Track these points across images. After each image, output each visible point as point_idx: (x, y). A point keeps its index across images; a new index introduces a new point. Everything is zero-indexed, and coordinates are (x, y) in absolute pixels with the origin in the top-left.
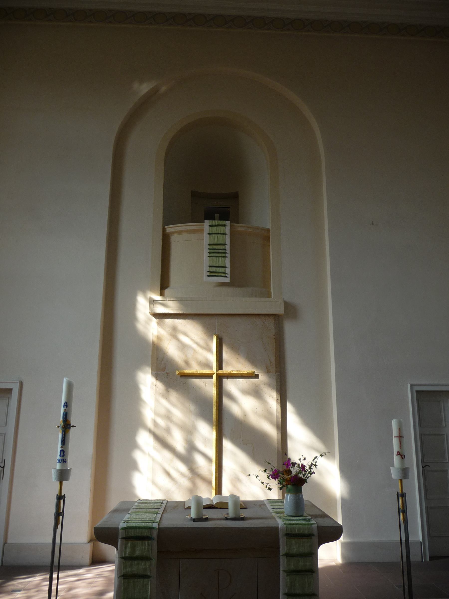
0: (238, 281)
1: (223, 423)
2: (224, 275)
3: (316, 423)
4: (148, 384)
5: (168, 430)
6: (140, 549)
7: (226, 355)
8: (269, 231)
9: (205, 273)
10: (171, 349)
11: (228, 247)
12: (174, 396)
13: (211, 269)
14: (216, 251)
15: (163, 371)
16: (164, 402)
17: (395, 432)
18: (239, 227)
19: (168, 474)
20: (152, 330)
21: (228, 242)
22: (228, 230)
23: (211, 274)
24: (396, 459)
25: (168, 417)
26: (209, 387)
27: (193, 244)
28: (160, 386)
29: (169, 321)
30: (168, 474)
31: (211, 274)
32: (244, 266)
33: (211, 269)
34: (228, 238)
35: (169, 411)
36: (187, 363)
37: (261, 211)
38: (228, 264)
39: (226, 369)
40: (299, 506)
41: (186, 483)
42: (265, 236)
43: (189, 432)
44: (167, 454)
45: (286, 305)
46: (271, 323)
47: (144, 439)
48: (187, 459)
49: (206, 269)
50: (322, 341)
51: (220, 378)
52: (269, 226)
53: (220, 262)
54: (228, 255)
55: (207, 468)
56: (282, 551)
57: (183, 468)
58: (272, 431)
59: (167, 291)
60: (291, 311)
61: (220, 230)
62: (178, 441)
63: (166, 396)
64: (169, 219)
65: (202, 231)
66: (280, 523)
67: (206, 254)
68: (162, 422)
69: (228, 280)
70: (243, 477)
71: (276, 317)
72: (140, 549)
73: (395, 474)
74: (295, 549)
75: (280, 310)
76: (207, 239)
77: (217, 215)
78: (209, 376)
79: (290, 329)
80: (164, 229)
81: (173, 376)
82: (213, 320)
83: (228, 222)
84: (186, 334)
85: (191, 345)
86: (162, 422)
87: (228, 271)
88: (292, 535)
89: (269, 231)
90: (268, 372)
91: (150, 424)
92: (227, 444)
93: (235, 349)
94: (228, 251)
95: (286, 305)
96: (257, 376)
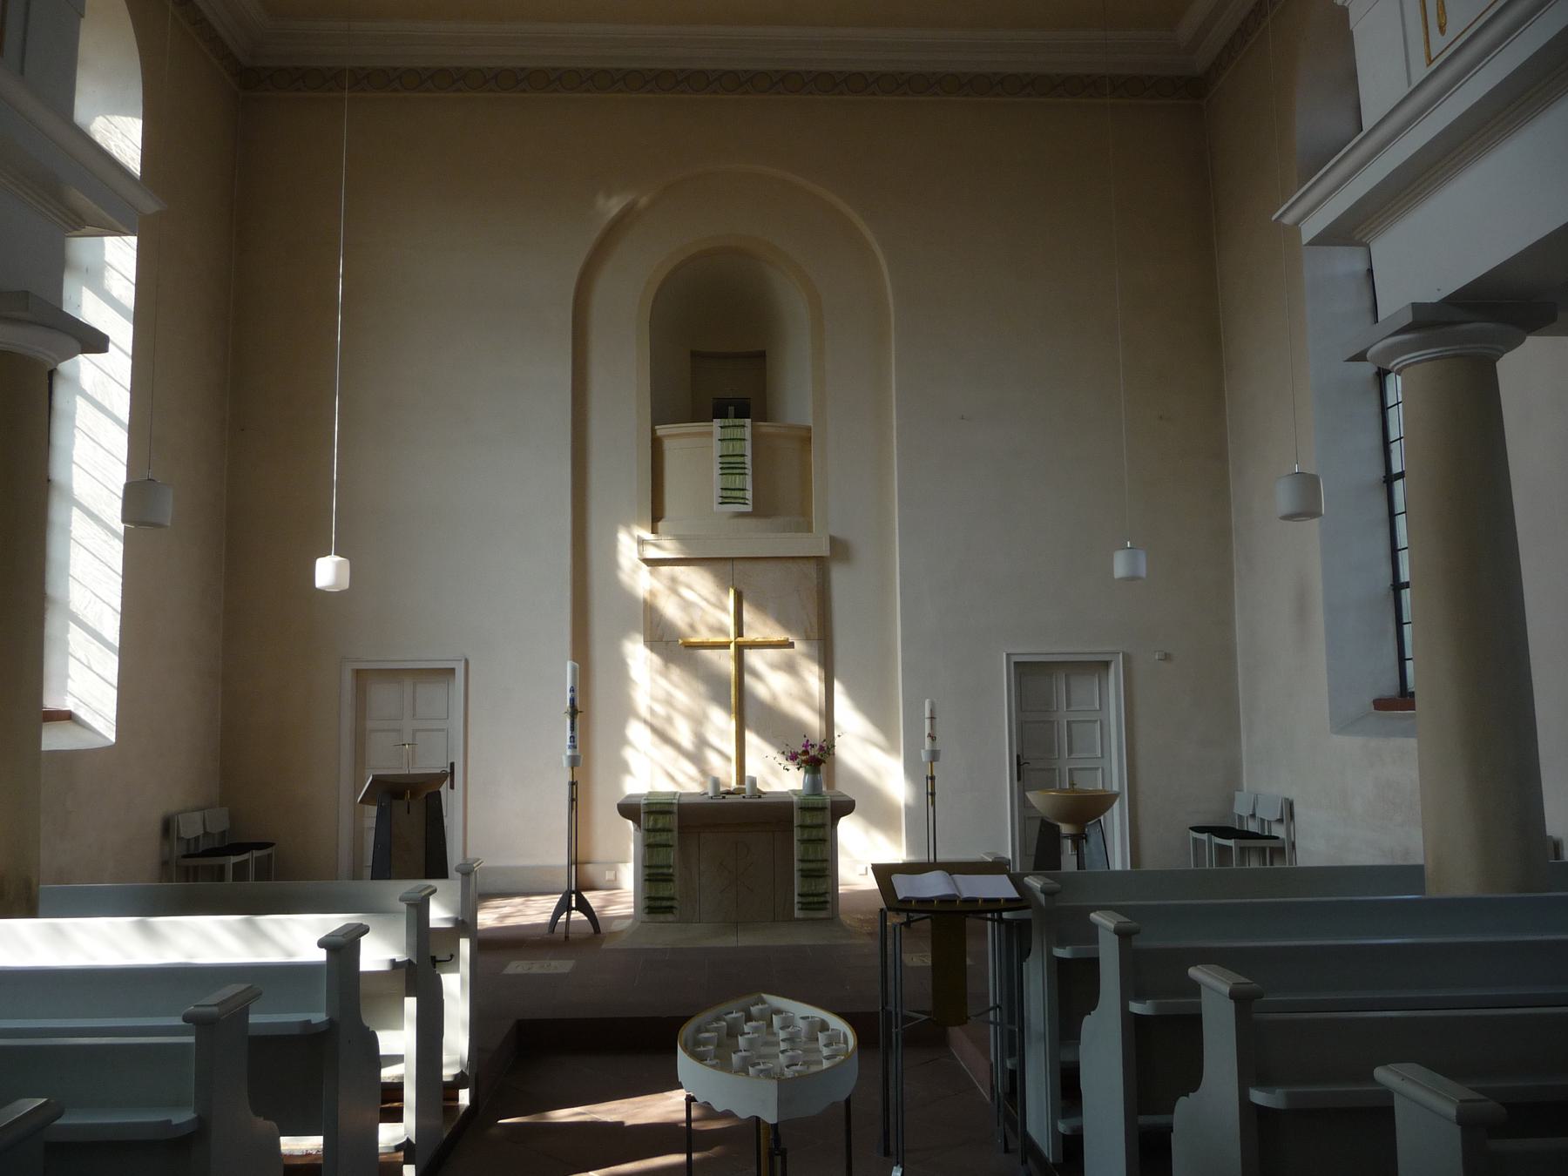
0: (764, 508)
3: (874, 708)
4: (638, 656)
5: (669, 720)
8: (809, 429)
9: (717, 500)
10: (670, 609)
11: (748, 460)
12: (676, 673)
14: (730, 466)
16: (662, 682)
17: (927, 714)
20: (642, 582)
21: (748, 452)
22: (748, 433)
24: (927, 741)
25: (669, 702)
26: (725, 661)
27: (697, 451)
28: (656, 660)
32: (773, 485)
34: (748, 444)
35: (669, 694)
37: (798, 396)
38: (749, 486)
39: (749, 636)
42: (804, 438)
43: (698, 721)
44: (669, 751)
45: (833, 541)
46: (811, 570)
51: (740, 649)
52: (810, 422)
53: (737, 481)
54: (749, 471)
56: (796, 823)
57: (692, 770)
58: (813, 721)
60: (840, 549)
61: (737, 433)
62: (683, 733)
64: (658, 418)
65: (710, 434)
67: (716, 471)
68: (660, 710)
69: (749, 508)
71: (819, 560)
75: (824, 550)
76: (717, 448)
78: (726, 646)
79: (840, 577)
80: (653, 431)
81: (673, 647)
82: (728, 566)
83: (748, 421)
84: (689, 587)
85: (698, 602)
86: (660, 710)
87: (749, 495)
88: (805, 809)
89: (809, 429)
91: (643, 711)
92: (750, 737)
93: (760, 607)
94: (749, 465)
95: (833, 541)
96: (791, 645)
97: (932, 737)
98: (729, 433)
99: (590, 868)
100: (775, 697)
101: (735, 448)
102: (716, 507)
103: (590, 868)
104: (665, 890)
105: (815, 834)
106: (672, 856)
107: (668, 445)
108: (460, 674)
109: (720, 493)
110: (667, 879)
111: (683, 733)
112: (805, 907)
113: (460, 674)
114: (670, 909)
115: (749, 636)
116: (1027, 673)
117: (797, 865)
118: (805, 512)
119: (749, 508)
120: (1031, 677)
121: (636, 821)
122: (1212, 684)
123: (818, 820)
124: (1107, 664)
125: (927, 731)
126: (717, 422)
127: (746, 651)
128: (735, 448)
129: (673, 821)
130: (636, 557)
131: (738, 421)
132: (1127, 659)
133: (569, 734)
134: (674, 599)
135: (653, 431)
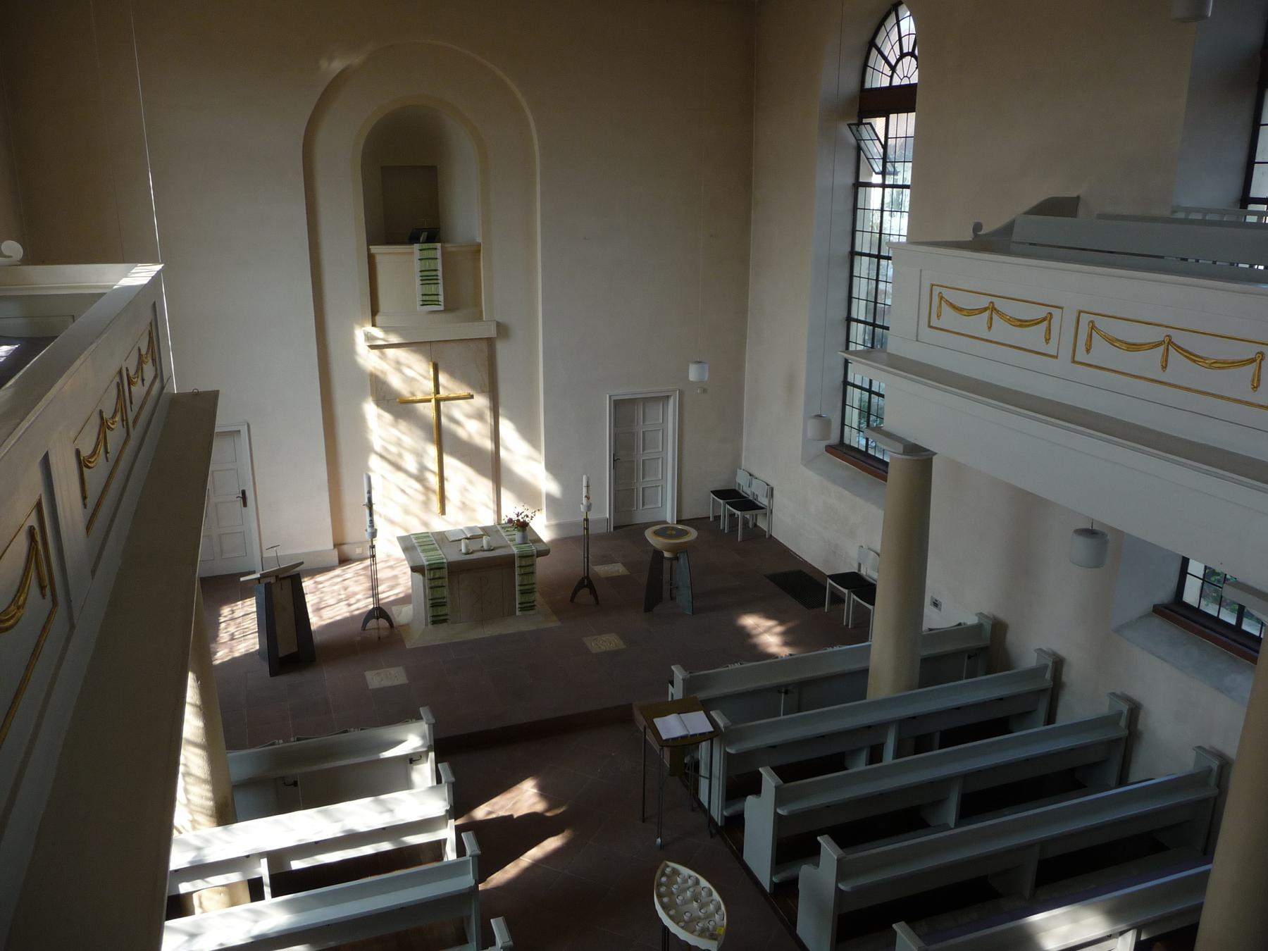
0: (451, 306)
1: (441, 437)
2: (436, 303)
3: (527, 432)
4: (370, 409)
5: (400, 456)
6: (438, 574)
7: (443, 379)
8: (479, 245)
9: (419, 303)
10: (396, 382)
11: (440, 273)
12: (403, 425)
13: (531, 569)
14: (428, 278)
15: (384, 399)
16: (394, 432)
17: (584, 484)
18: (450, 247)
19: (403, 491)
20: (369, 360)
21: (440, 268)
22: (439, 254)
23: (425, 303)
24: (584, 500)
25: (399, 444)
26: (428, 410)
27: (401, 266)
28: (388, 417)
29: (390, 352)
30: (403, 491)
31: (425, 303)
32: (455, 290)
33: (531, 569)
34: (439, 262)
35: (399, 439)
36: (413, 394)
37: (467, 215)
38: (441, 292)
39: (443, 393)
40: (524, 540)
41: (421, 498)
42: (475, 251)
43: (419, 455)
44: (401, 475)
45: (498, 325)
46: (484, 346)
47: (374, 461)
48: (420, 479)
49: (419, 298)
50: (532, 358)
51: (438, 402)
52: (479, 239)
53: (433, 289)
54: (441, 281)
55: (434, 481)
56: (517, 565)
57: (417, 486)
58: (488, 445)
59: (378, 318)
60: (503, 330)
61: (431, 254)
62: (411, 464)
63: (395, 425)
64: (373, 239)
65: (412, 253)
66: (515, 550)
67: (418, 282)
68: (394, 449)
69: (441, 308)
70: (469, 487)
71: (490, 342)
72: (438, 574)
73: (583, 508)
74: (524, 563)
75: (492, 332)
76: (417, 266)
77: (424, 236)
78: (429, 401)
79: (502, 349)
80: (369, 250)
81: (398, 406)
82: (428, 347)
83: (439, 245)
84: (409, 367)
85: (409, 372)
86: (394, 449)
87: (441, 298)
88: (522, 557)
89: (479, 245)
90: (481, 391)
91: (377, 447)
92: (447, 459)
93: (452, 374)
94: (440, 277)
95: (498, 325)
96: (472, 397)
97: (588, 497)
98: (426, 254)
99: (345, 548)
100: (470, 436)
101: (431, 264)
102: (419, 308)
103: (345, 548)
104: (441, 611)
105: (527, 570)
106: (446, 592)
107: (379, 259)
108: (244, 430)
109: (421, 298)
110: (443, 604)
111: (411, 465)
112: (522, 609)
113: (244, 430)
114: (445, 621)
115: (443, 393)
116: (618, 405)
117: (517, 588)
118: (477, 303)
119: (441, 308)
120: (623, 410)
121: (423, 575)
122: (727, 402)
123: (529, 562)
124: (668, 397)
125: (584, 493)
126: (416, 247)
127: (442, 403)
128: (431, 264)
129: (445, 572)
130: (375, 351)
131: (431, 245)
132: (681, 394)
133: (368, 519)
134: (398, 375)
135: (369, 250)
